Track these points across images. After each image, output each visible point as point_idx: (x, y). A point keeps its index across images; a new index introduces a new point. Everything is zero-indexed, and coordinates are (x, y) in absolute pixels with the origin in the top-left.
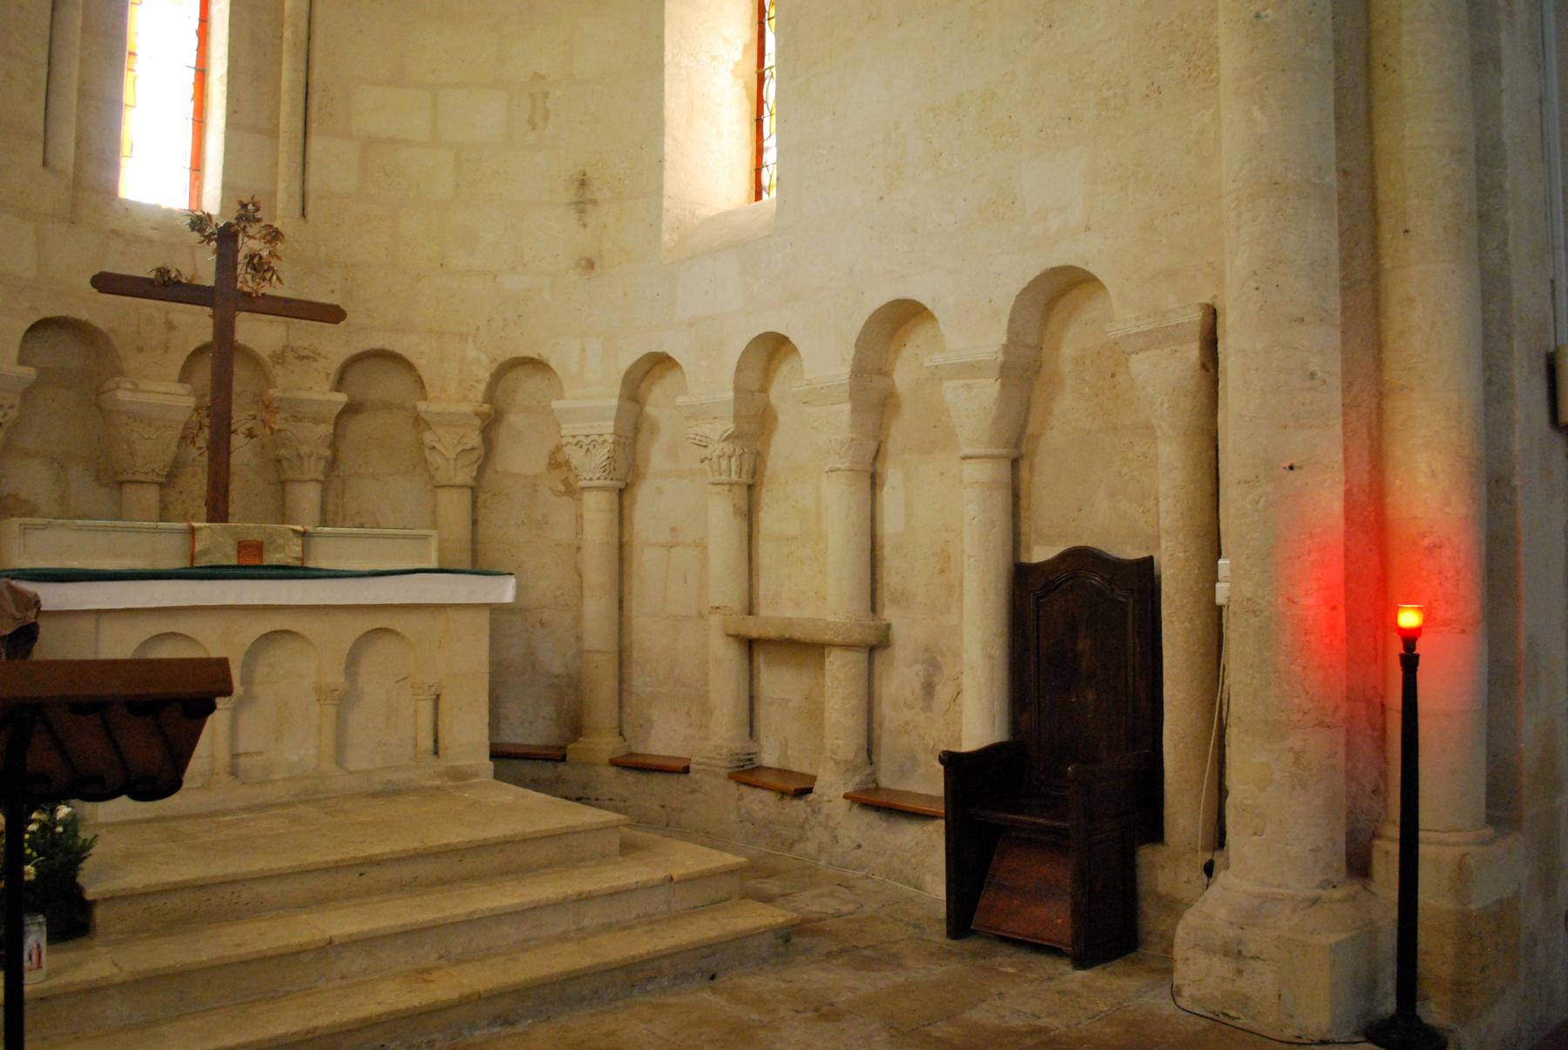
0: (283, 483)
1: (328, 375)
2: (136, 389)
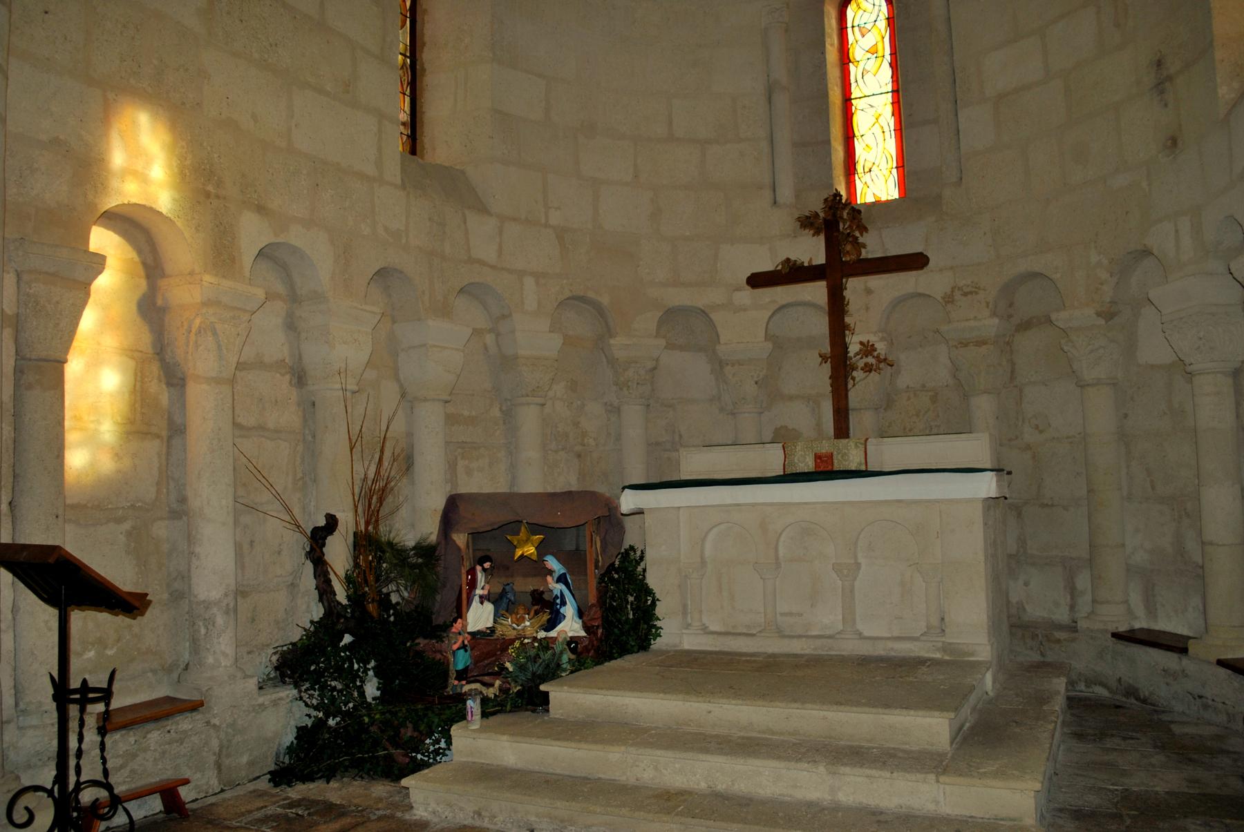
1: (988, 304)
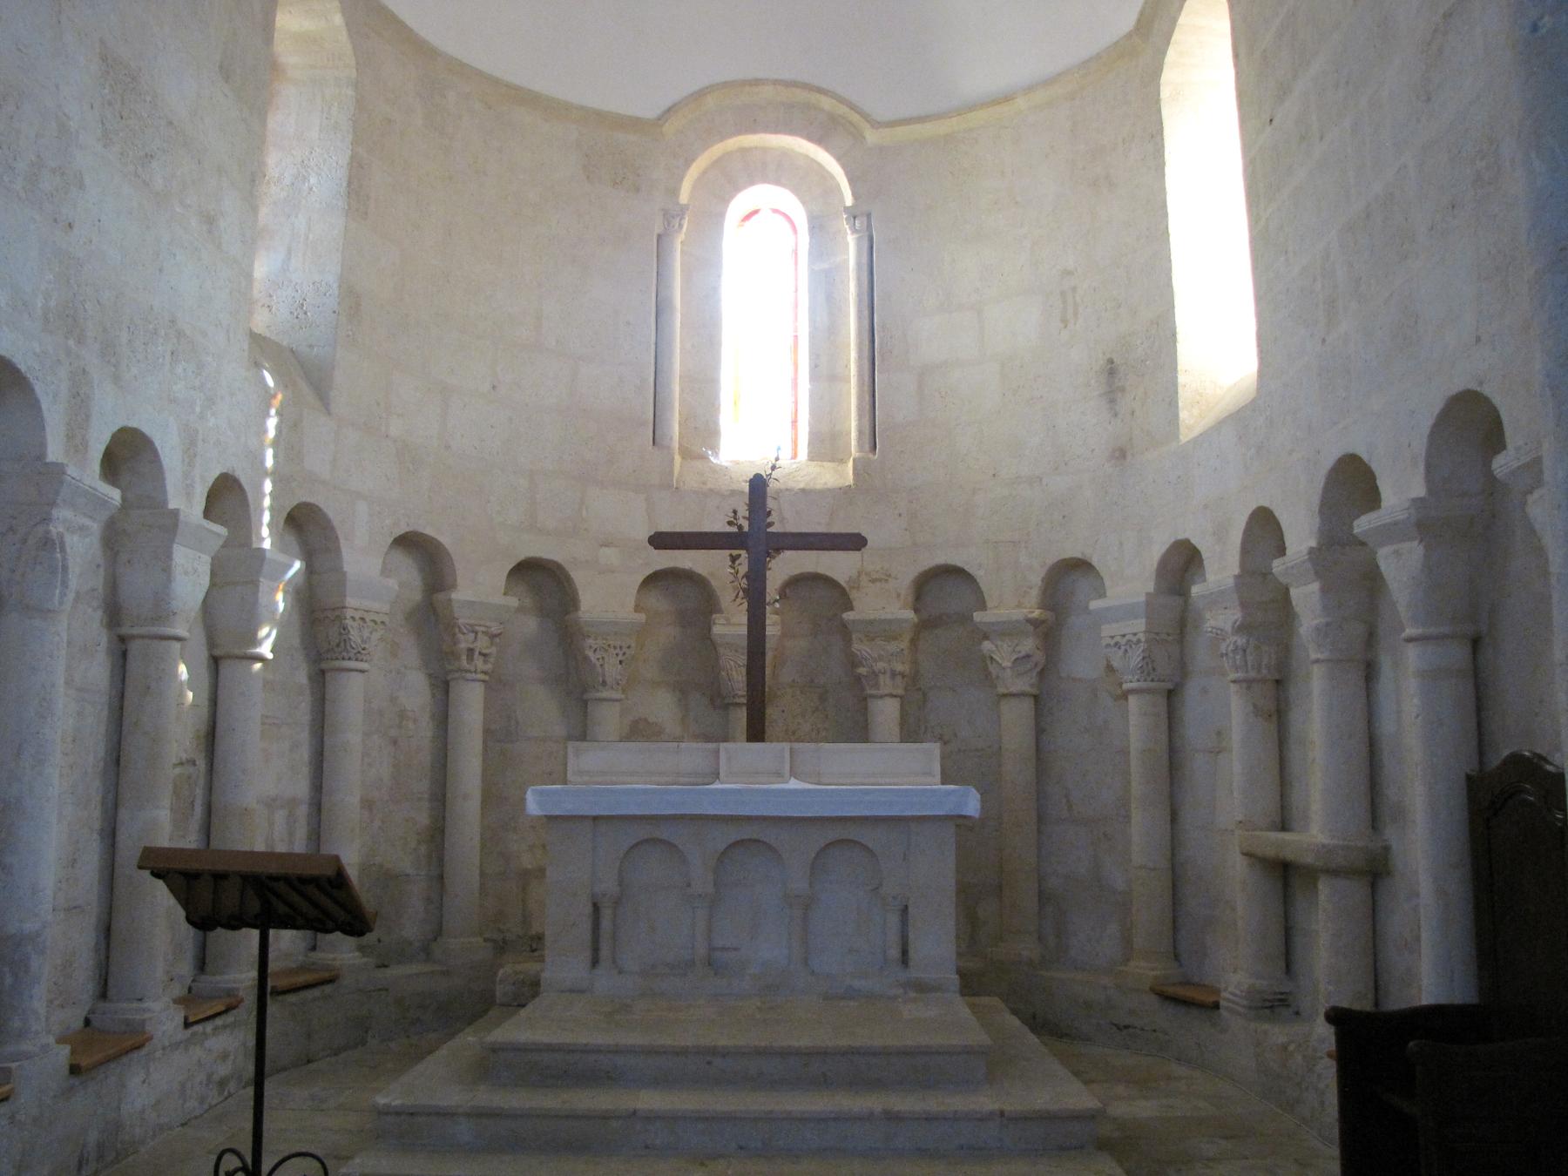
0: (865, 699)
1: (899, 595)
2: (728, 623)
